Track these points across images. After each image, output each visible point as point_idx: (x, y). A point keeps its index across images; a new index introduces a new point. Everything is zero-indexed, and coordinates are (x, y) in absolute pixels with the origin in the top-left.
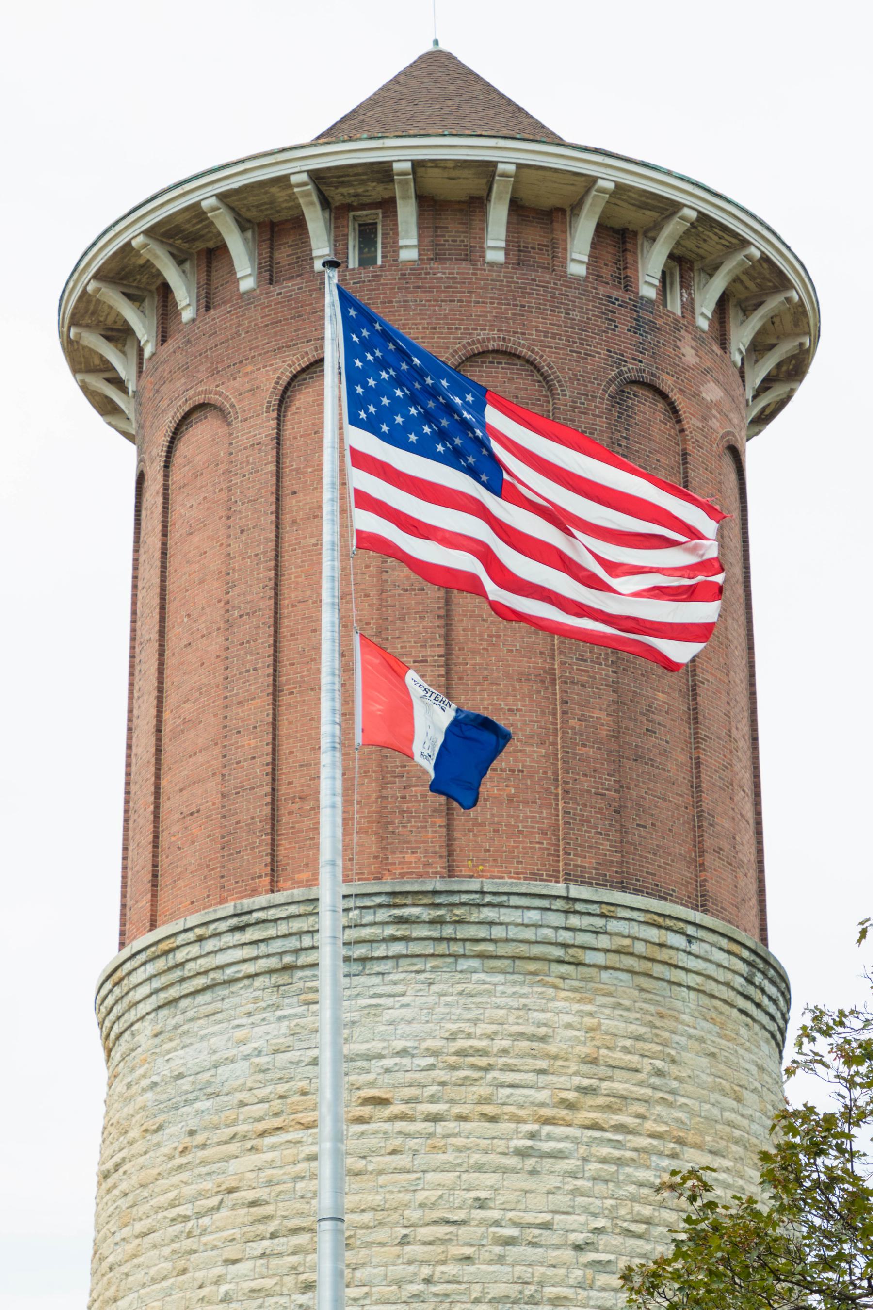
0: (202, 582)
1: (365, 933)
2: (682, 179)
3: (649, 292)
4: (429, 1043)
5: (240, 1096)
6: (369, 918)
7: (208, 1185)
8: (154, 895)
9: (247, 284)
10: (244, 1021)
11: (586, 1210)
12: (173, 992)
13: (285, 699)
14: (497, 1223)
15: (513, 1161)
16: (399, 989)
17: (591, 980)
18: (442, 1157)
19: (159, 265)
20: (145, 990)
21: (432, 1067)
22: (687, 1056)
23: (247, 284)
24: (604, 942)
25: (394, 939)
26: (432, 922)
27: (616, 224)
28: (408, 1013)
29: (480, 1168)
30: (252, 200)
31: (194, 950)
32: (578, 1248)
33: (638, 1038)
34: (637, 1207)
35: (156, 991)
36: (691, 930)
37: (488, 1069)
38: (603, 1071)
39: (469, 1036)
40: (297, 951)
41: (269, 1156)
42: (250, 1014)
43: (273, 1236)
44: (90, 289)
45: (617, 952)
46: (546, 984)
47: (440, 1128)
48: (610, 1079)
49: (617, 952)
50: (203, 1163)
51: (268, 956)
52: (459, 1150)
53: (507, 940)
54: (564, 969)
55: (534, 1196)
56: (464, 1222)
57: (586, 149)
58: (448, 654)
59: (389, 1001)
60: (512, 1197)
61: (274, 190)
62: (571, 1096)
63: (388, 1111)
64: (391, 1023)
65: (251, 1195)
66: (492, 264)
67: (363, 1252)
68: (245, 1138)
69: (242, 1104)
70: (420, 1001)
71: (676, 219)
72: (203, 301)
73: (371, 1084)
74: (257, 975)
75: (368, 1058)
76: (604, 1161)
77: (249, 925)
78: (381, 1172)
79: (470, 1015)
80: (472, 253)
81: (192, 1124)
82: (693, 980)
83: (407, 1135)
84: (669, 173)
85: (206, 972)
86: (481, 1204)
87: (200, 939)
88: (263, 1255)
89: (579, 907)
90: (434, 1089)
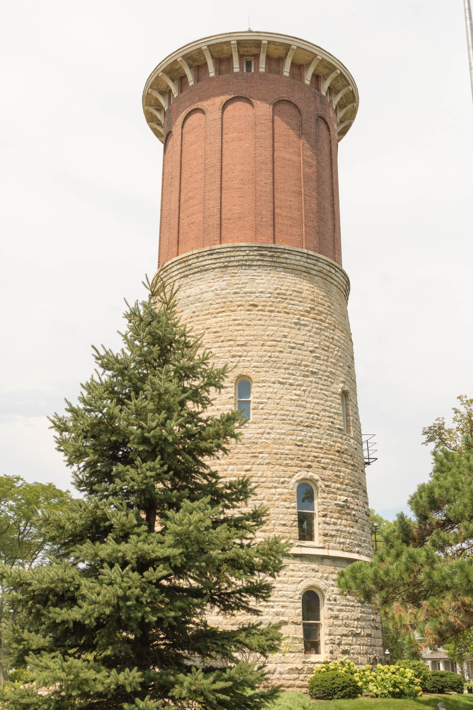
0: (195, 159)
1: (251, 257)
2: (338, 60)
3: (324, 94)
4: (269, 290)
5: (210, 302)
6: (252, 253)
7: (200, 327)
8: (178, 247)
9: (212, 75)
10: (211, 281)
11: (313, 342)
12: (187, 273)
13: (223, 191)
14: (289, 342)
15: (293, 325)
16: (260, 274)
17: (312, 278)
18: (274, 322)
19: (184, 68)
20: (177, 272)
21: (270, 297)
22: (335, 304)
23: (212, 75)
24: (316, 268)
25: (259, 260)
26: (270, 256)
27: (316, 74)
28: (263, 281)
29: (284, 327)
30: (217, 49)
31: (195, 260)
32: (311, 352)
33: (324, 296)
34: (325, 343)
35: (180, 273)
36: (336, 269)
37: (286, 299)
38: (316, 304)
39: (281, 289)
40: (229, 262)
41: (221, 319)
42: (213, 279)
43: (222, 342)
44: (160, 75)
45: (319, 271)
46: (301, 278)
47: (272, 314)
48: (318, 306)
49: (319, 271)
50: (198, 321)
51: (220, 263)
52: (278, 321)
53: (291, 264)
54: (306, 274)
55: (300, 336)
56: (280, 341)
57: (315, 46)
58: (273, 182)
59: (257, 278)
60: (294, 335)
61: (224, 46)
62: (308, 309)
63: (257, 309)
64: (258, 284)
65: (215, 330)
66: (285, 76)
67: (250, 347)
68: (212, 314)
69: (211, 304)
70: (266, 278)
71: (334, 73)
72: (196, 80)
73: (252, 300)
74: (216, 268)
75: (251, 293)
76: (317, 328)
77: (214, 253)
78: (256, 325)
79: (281, 284)
80: (280, 72)
81: (194, 310)
82: (336, 283)
83: (263, 315)
84: (335, 58)
85: (198, 267)
86: (285, 336)
87: (197, 257)
88: (219, 347)
89: (310, 257)
90: (271, 303)
